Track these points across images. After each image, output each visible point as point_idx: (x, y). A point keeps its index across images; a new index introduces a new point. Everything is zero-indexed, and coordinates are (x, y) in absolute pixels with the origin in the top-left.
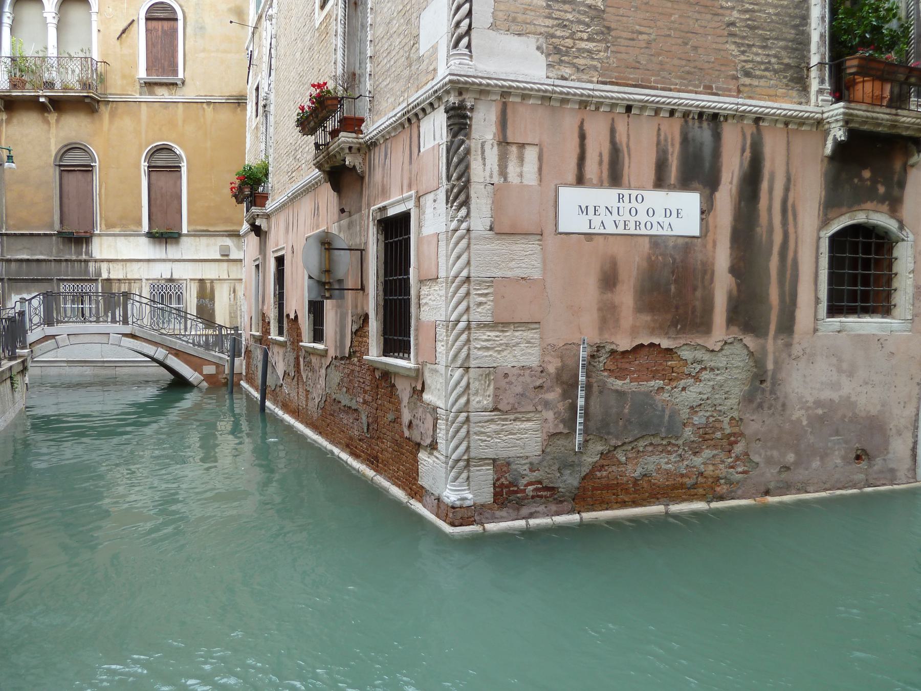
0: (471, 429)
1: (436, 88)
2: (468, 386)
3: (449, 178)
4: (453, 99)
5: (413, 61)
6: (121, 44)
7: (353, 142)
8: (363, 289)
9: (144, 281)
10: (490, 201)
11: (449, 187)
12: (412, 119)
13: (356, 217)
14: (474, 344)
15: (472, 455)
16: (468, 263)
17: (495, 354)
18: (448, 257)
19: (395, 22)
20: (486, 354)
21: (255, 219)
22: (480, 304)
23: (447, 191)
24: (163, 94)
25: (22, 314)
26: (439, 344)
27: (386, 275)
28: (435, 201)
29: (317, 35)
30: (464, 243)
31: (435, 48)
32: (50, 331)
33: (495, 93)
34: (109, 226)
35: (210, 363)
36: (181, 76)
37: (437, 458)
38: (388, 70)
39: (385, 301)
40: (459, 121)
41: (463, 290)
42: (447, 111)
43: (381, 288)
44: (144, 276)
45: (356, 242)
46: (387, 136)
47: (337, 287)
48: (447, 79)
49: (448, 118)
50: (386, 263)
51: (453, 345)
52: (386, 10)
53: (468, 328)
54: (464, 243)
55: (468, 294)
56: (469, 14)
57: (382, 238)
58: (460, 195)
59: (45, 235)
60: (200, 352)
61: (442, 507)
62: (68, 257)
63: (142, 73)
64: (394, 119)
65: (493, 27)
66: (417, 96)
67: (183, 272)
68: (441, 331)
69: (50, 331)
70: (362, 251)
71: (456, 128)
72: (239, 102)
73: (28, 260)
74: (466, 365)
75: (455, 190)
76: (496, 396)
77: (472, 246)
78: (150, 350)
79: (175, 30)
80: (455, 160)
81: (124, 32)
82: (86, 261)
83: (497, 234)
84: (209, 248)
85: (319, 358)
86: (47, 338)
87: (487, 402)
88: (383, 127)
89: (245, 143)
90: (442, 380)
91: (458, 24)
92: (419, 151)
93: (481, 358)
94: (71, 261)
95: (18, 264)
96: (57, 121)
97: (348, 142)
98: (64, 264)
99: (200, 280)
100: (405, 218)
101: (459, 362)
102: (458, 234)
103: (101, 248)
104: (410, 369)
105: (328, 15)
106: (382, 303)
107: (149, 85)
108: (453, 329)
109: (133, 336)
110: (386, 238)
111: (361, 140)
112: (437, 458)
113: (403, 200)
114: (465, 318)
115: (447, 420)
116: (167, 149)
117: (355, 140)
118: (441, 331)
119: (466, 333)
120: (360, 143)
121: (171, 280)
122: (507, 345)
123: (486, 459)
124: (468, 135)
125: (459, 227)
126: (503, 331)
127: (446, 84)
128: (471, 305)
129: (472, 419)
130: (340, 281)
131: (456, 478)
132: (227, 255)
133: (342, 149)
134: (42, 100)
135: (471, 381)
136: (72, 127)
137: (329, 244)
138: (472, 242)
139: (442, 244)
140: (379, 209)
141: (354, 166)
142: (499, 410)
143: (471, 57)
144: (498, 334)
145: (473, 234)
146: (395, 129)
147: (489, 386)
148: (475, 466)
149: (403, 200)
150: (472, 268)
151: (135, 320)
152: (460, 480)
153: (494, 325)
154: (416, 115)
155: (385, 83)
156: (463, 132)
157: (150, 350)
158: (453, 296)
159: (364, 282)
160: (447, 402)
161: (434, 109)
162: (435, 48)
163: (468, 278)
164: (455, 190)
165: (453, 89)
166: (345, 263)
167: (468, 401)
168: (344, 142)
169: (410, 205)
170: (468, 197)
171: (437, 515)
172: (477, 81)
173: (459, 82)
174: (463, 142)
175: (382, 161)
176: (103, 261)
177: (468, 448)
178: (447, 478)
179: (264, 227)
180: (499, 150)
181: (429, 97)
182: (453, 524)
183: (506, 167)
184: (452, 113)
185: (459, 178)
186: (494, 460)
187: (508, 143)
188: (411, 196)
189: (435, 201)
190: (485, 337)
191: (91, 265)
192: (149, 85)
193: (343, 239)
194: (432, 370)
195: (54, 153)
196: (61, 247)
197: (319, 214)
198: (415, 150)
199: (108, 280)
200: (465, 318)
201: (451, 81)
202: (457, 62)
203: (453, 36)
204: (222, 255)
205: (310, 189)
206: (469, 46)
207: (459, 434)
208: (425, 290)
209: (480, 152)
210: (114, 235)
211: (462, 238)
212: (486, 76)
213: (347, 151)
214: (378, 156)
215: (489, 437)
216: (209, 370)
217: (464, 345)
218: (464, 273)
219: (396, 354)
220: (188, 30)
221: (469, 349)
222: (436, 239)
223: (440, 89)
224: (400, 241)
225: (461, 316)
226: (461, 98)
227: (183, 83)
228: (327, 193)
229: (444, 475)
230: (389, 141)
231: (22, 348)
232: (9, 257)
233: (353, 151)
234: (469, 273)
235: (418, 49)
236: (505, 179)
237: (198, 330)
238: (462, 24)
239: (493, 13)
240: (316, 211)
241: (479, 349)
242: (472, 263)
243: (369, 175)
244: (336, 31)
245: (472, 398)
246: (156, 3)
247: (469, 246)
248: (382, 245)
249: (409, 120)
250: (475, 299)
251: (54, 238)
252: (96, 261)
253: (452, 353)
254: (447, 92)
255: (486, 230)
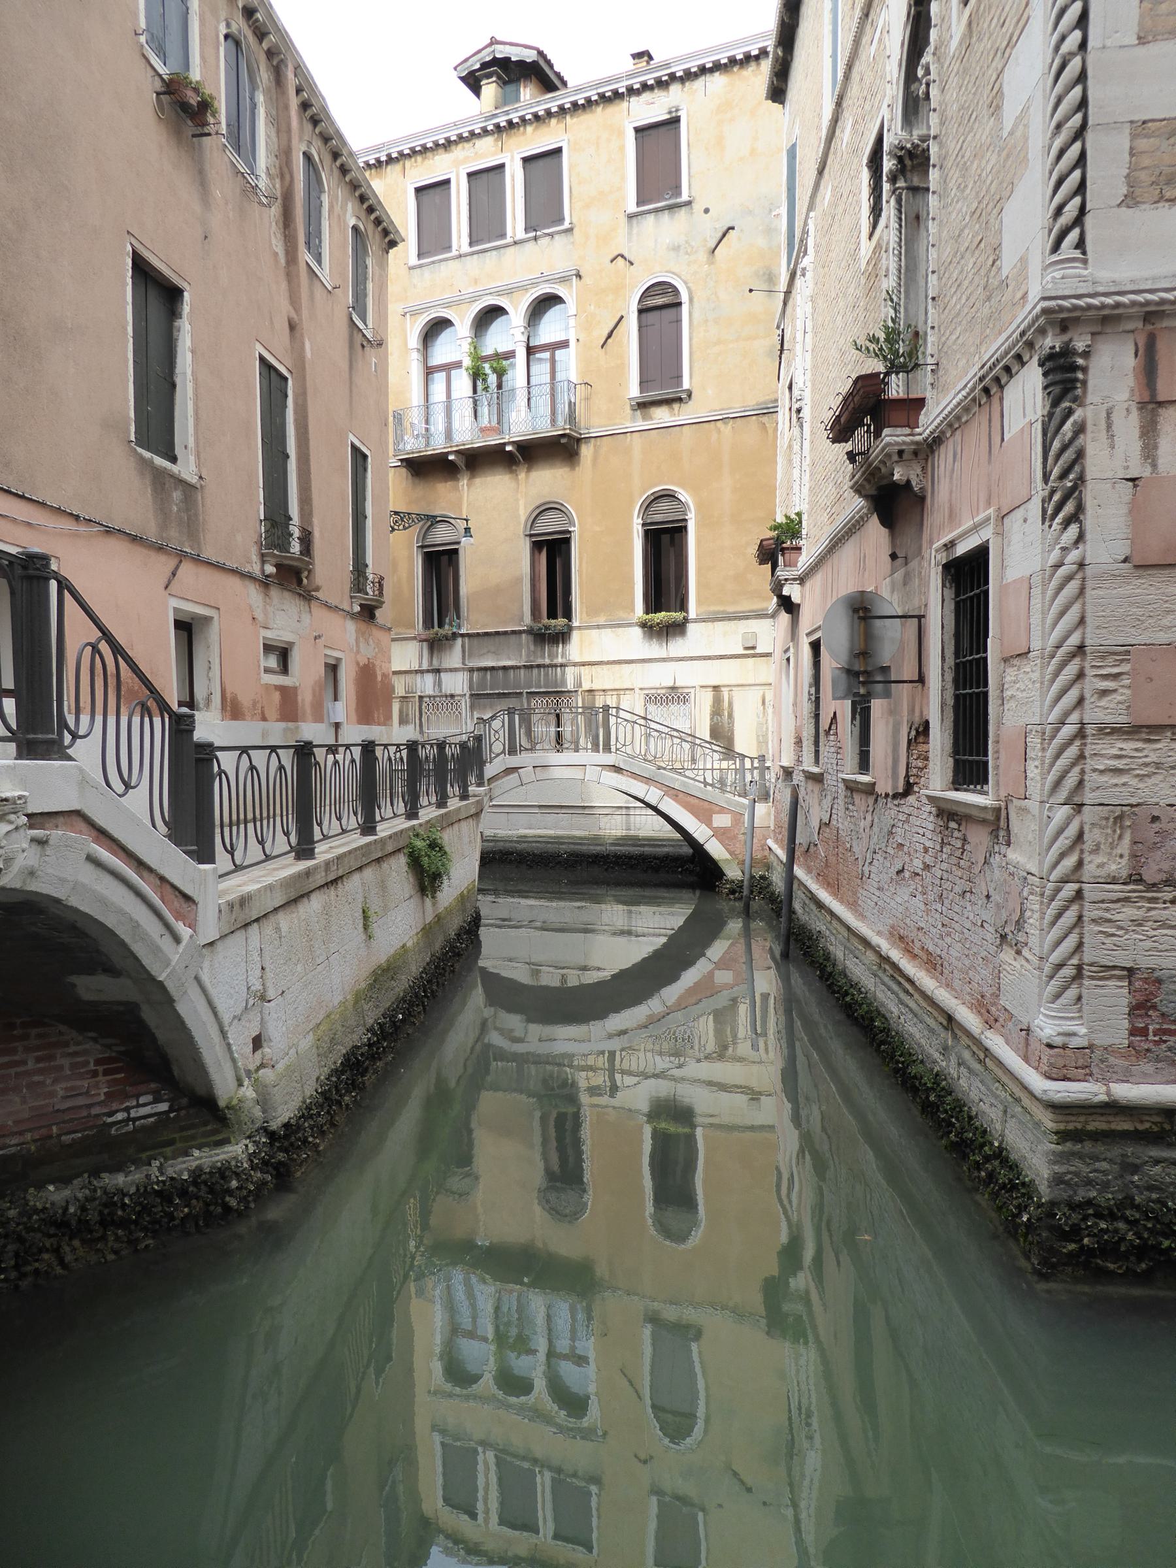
0: (1085, 913)
1: (1022, 327)
2: (1080, 837)
3: (1046, 478)
4: (1051, 341)
5: (994, 288)
6: (606, 353)
7: (904, 443)
8: (921, 680)
9: (637, 690)
10: (1124, 510)
11: (1046, 493)
12: (991, 387)
13: (914, 564)
14: (1090, 763)
15: (1088, 956)
16: (1082, 621)
17: (1134, 782)
18: (1044, 613)
19: (966, 231)
20: (1115, 781)
21: (782, 586)
22: (1104, 693)
23: (1043, 501)
24: (662, 416)
25: (479, 739)
26: (1031, 765)
27: (957, 654)
28: (1025, 521)
29: (863, 281)
30: (1074, 585)
31: (1023, 261)
32: (513, 761)
33: (1130, 317)
34: (592, 611)
35: (723, 810)
36: (686, 385)
37: (1027, 960)
38: (958, 314)
39: (957, 697)
40: (1064, 377)
41: (1071, 669)
42: (1041, 365)
43: (949, 677)
44: (637, 685)
45: (912, 608)
46: (955, 423)
47: (879, 678)
48: (1038, 308)
49: (1045, 375)
50: (957, 635)
51: (1052, 765)
52: (954, 215)
53: (1081, 734)
54: (1074, 585)
55: (1081, 675)
56: (1081, 188)
57: (950, 594)
58: (1067, 501)
59: (514, 632)
60: (711, 794)
61: (1034, 1045)
62: (540, 661)
63: (634, 391)
64: (964, 393)
65: (1130, 200)
66: (995, 346)
67: (688, 676)
68: (1034, 741)
69: (513, 761)
70: (920, 617)
71: (1057, 390)
72: (768, 411)
73: (493, 668)
74: (1077, 800)
75: (1056, 497)
76: (1134, 856)
77: (1089, 592)
78: (639, 789)
79: (679, 321)
80: (1056, 445)
81: (610, 336)
82: (562, 666)
83: (1137, 567)
84: (726, 637)
85: (864, 796)
86: (510, 771)
87: (1119, 867)
88: (949, 409)
89: (776, 472)
90: (1034, 826)
91: (1059, 211)
92: (1003, 440)
93: (1104, 789)
94: (544, 666)
95: (481, 674)
96: (527, 477)
97: (897, 443)
98: (535, 671)
99: (715, 687)
100: (980, 556)
101: (1063, 794)
102: (1062, 572)
103: (579, 647)
104: (985, 808)
105: (878, 246)
106: (950, 702)
107: (643, 406)
108: (1053, 737)
109: (617, 769)
110: (957, 594)
111: (918, 438)
112: (1027, 960)
113: (976, 528)
114: (1074, 717)
115: (1042, 895)
116: (669, 496)
117: (907, 439)
118: (1034, 741)
119: (1078, 743)
120: (917, 443)
121: (673, 688)
122: (1158, 765)
123: (1114, 967)
124: (1079, 401)
125: (1063, 557)
126: (1149, 741)
127: (1037, 317)
128: (1087, 695)
129: (1086, 894)
130: (885, 670)
131: (1057, 996)
132: (753, 648)
133: (889, 455)
134: (509, 448)
135: (1086, 828)
136: (545, 481)
137: (866, 610)
138: (1089, 584)
139: (1036, 592)
140: (945, 545)
141: (908, 481)
142: (1140, 881)
143: (1085, 262)
144: (1140, 745)
145: (1089, 571)
146: (967, 409)
147: (1120, 837)
148: (1092, 978)
149: (976, 528)
150: (1088, 630)
151: (619, 746)
152: (1062, 1000)
153: (1133, 731)
154: (997, 380)
155: (954, 337)
156: (1070, 396)
157: (639, 789)
158: (1053, 681)
159: (924, 669)
160: (1041, 863)
161: (1023, 364)
162: (1023, 261)
163: (1081, 649)
164: (1056, 497)
165: (1051, 323)
166: (893, 641)
167: (1080, 864)
168: (888, 444)
169: (986, 534)
170: (1080, 508)
171: (1026, 1059)
172: (1094, 302)
173: (1061, 309)
174: (1069, 412)
175: (949, 467)
176: (583, 664)
177: (1080, 945)
178: (1040, 995)
179: (796, 599)
180: (1142, 418)
181: (1014, 346)
182: (1049, 1077)
183: (1156, 447)
184: (1048, 365)
185: (1063, 476)
186: (1131, 971)
187: (1161, 404)
188: (988, 519)
189: (1025, 521)
190: (1115, 752)
191: (569, 671)
192: (643, 406)
193: (891, 601)
194: (1020, 808)
195: (523, 519)
196: (532, 648)
197: (867, 564)
198: (996, 439)
199: (590, 691)
200: (1074, 717)
201: (1045, 311)
202: (1058, 275)
203: (1050, 231)
204: (747, 648)
205: (852, 529)
206: (1081, 244)
207: (1062, 920)
208: (1011, 674)
209: (1103, 425)
210: (598, 627)
211: (1069, 578)
212: (1113, 289)
213: (895, 458)
214: (944, 458)
215: (1121, 928)
216: (722, 821)
217: (1073, 765)
218: (1074, 640)
219: (972, 787)
220: (696, 315)
221: (1083, 772)
222: (1026, 586)
223: (1029, 327)
224: (971, 598)
225: (1067, 714)
226: (1065, 338)
227: (690, 394)
228: (875, 530)
229: (1037, 990)
230: (958, 432)
231: (480, 784)
232: (471, 665)
233: (905, 456)
234: (1083, 638)
235: (1000, 269)
236: (1154, 466)
237: (713, 762)
238: (1067, 208)
239: (1127, 176)
240: (862, 561)
241: (1102, 772)
242: (1088, 620)
243: (933, 493)
244: (887, 270)
245: (1087, 858)
246: (653, 285)
247: (1082, 591)
248: (950, 606)
249: (986, 390)
250: (1092, 683)
251: (524, 636)
252: (575, 665)
253: (1051, 778)
254: (1042, 331)
255: (1116, 561)
